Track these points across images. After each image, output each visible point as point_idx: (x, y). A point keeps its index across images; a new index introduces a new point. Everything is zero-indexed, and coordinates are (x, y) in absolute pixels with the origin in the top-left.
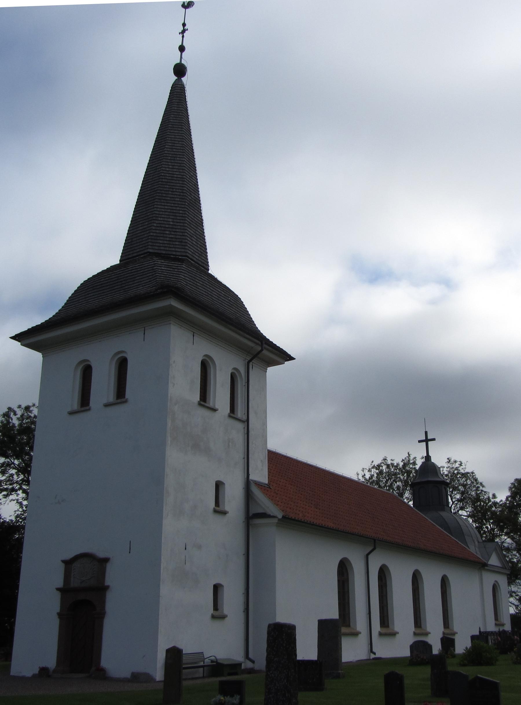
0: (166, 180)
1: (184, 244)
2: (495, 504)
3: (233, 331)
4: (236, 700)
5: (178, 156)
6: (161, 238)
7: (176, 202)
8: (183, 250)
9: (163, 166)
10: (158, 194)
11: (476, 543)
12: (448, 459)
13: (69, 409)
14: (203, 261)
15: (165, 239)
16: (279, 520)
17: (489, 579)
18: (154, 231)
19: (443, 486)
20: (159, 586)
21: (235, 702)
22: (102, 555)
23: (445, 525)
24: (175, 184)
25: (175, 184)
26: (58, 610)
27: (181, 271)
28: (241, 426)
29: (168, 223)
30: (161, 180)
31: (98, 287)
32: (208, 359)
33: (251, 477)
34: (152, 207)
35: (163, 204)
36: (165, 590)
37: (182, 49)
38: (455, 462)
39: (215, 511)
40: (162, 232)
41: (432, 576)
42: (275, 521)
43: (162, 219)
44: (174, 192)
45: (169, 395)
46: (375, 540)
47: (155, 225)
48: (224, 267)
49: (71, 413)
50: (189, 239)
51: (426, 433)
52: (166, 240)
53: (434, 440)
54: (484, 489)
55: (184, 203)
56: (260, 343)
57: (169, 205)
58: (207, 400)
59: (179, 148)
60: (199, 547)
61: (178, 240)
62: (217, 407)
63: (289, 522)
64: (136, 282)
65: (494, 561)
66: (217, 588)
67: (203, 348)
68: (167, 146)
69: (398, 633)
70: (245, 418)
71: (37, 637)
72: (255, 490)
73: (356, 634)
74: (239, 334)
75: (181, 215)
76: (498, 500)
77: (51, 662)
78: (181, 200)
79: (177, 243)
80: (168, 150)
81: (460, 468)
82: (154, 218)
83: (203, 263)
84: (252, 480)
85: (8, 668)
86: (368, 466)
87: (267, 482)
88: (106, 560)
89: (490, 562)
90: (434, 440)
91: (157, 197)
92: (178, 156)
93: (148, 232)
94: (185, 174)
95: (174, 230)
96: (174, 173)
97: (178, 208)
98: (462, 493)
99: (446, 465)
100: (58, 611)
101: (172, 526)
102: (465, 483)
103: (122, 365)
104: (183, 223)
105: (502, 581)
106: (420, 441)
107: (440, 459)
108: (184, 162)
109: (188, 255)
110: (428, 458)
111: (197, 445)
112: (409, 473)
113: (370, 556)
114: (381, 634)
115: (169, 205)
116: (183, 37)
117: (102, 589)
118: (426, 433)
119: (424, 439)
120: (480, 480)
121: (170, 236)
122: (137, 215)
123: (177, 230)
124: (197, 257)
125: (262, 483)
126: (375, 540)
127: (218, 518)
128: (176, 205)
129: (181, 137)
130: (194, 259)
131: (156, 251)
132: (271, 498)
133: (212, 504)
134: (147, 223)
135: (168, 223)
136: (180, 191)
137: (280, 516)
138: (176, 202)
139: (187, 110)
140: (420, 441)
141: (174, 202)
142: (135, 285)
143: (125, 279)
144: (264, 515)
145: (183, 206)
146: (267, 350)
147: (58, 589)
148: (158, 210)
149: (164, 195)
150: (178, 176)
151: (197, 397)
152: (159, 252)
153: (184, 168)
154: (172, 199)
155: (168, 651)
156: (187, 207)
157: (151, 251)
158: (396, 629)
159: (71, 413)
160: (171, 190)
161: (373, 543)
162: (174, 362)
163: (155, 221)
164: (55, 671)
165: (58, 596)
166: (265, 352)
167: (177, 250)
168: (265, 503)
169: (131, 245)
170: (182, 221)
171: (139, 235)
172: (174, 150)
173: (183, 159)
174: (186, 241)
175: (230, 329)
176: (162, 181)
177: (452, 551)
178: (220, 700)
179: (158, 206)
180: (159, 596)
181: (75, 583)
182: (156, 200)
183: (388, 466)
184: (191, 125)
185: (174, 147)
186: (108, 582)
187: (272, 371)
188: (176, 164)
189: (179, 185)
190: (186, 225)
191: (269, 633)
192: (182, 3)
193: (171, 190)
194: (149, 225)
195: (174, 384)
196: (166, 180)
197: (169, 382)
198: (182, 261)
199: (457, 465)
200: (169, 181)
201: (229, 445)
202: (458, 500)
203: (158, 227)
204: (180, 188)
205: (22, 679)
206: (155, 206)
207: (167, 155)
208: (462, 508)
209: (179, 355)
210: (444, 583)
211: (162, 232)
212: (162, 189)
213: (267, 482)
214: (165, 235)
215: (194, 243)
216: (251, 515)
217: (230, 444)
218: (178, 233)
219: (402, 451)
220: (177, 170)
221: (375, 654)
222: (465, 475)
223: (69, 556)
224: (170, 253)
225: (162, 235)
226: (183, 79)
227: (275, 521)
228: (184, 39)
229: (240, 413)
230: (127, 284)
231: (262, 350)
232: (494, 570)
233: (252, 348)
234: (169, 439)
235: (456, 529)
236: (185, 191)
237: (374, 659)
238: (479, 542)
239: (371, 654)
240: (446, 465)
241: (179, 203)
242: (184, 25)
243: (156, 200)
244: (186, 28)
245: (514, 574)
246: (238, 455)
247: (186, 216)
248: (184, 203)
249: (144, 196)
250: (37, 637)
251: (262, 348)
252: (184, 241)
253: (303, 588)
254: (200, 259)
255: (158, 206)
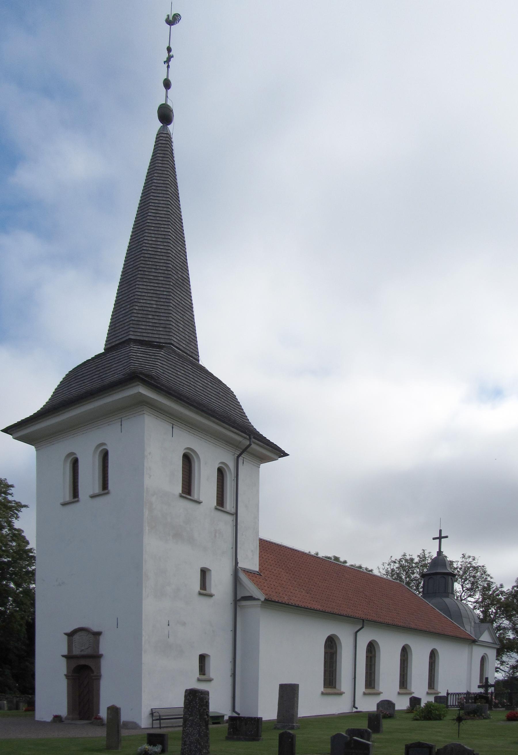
0: (149, 256)
1: (168, 330)
2: (502, 593)
3: (217, 424)
4: (158, 749)
5: (162, 226)
6: (144, 323)
7: (160, 282)
8: (167, 337)
9: (146, 238)
10: (140, 272)
11: (473, 623)
12: (463, 554)
13: (62, 501)
14: (192, 350)
15: (148, 324)
16: (262, 602)
17: (478, 652)
18: (136, 315)
19: (450, 577)
20: (141, 655)
21: (156, 750)
22: (95, 629)
23: (447, 610)
24: (159, 261)
25: (159, 261)
26: (65, 672)
27: (158, 357)
28: (229, 519)
29: (151, 306)
30: (142, 255)
31: (79, 377)
32: (190, 452)
33: (240, 565)
34: (134, 288)
35: (145, 284)
36: (148, 659)
37: (167, 84)
38: (469, 557)
39: (200, 594)
40: (144, 316)
41: (420, 651)
42: (259, 603)
43: (144, 301)
44: (157, 269)
45: (145, 487)
46: (363, 620)
47: (137, 308)
48: (214, 357)
49: (64, 504)
50: (174, 324)
51: (440, 531)
52: (149, 326)
53: (446, 537)
54: (492, 580)
55: (168, 283)
56: (248, 437)
57: (152, 284)
58: (192, 493)
59: (163, 216)
60: (184, 624)
61: (162, 326)
62: (201, 499)
63: (270, 603)
64: (112, 370)
65: (486, 637)
66: (203, 658)
67: (183, 441)
68: (150, 214)
69: (382, 693)
70: (233, 511)
71: (52, 692)
72: (242, 576)
73: (341, 694)
74: (224, 428)
75: (165, 297)
76: (505, 589)
77: (63, 712)
78: (165, 279)
79: (161, 329)
80: (151, 218)
81: (472, 563)
82: (136, 300)
83: (192, 352)
84: (240, 568)
85: (34, 716)
86: (387, 561)
87: (257, 570)
88: (99, 634)
89: (482, 639)
90: (446, 537)
91: (139, 276)
92: (162, 226)
93: (129, 316)
94: (169, 248)
95: (158, 314)
96: (158, 247)
97: (162, 289)
98: (473, 584)
99: (461, 560)
100: (65, 673)
101: (150, 605)
102: (474, 575)
103: (105, 456)
104: (168, 306)
105: (492, 654)
106: (434, 539)
107: (454, 555)
108: (170, 234)
109: (173, 342)
110: (440, 553)
111: (178, 534)
112: (425, 565)
113: (358, 633)
114: (365, 694)
115: (152, 284)
116: (168, 67)
117: (97, 657)
118: (440, 531)
119: (438, 536)
120: (488, 572)
121: (154, 321)
122: (120, 297)
123: (161, 314)
124: (184, 346)
125: (253, 571)
126: (363, 620)
127: (204, 600)
128: (160, 285)
129: (166, 202)
130: (181, 347)
131: (138, 338)
132: (257, 584)
133: (197, 587)
134: (129, 306)
135: (151, 306)
136: (164, 268)
137: (263, 599)
138: (160, 282)
139: (174, 168)
140: (434, 539)
141: (157, 282)
142: (111, 373)
143: (103, 367)
144: (250, 598)
145: (168, 287)
146: (255, 443)
147: (63, 656)
148: (140, 290)
149: (147, 273)
150: (163, 251)
151: (178, 489)
152: (142, 338)
153: (169, 241)
154: (156, 278)
155: (109, 708)
156: (172, 287)
157: (133, 337)
158: (381, 690)
159: (64, 504)
160: (155, 267)
161: (363, 622)
162: (150, 453)
163: (136, 304)
164: (66, 718)
165: (63, 662)
166: (253, 446)
167: (160, 336)
168: (251, 588)
169: (115, 331)
170: (166, 304)
171: (122, 320)
172: (158, 219)
173: (168, 230)
174: (171, 327)
175: (214, 422)
176: (144, 257)
177: (452, 630)
178: (145, 748)
179: (140, 287)
180: (141, 664)
181: (76, 652)
182: (138, 279)
183: (406, 561)
184: (179, 188)
185: (157, 215)
186: (102, 651)
187: (265, 467)
188: (160, 236)
189: (163, 261)
190: (171, 308)
191: (186, 696)
192: (166, 17)
193: (155, 267)
194: (131, 308)
195: (150, 476)
196: (149, 256)
197: (145, 473)
198: (160, 347)
199: (471, 560)
200: (152, 256)
201: (215, 536)
202: (468, 589)
203: (140, 310)
204: (165, 265)
205: (44, 723)
206: (137, 286)
207: (150, 225)
208: (470, 596)
209: (155, 447)
210: (433, 655)
211: (144, 316)
212: (144, 266)
213: (257, 570)
214: (148, 320)
215: (181, 329)
216: (238, 598)
217: (217, 535)
218: (163, 318)
219: (420, 547)
220: (161, 244)
221: (357, 708)
222: (476, 569)
223: (69, 630)
224: (153, 340)
225: (144, 320)
226: (170, 127)
227: (259, 603)
228: (170, 69)
229: (229, 505)
230: (104, 373)
231: (250, 445)
232: (485, 645)
233: (240, 442)
234: (146, 529)
235: (456, 614)
236: (169, 269)
237: (355, 712)
238: (475, 623)
239: (354, 709)
240: (461, 560)
241: (163, 282)
242: (169, 50)
243: (138, 279)
244: (171, 54)
245: (503, 647)
246: (227, 545)
247: (171, 297)
248: (168, 283)
249: (126, 275)
250: (52, 692)
251: (250, 441)
252: (168, 326)
253: (287, 658)
254: (187, 348)
255: (140, 287)
